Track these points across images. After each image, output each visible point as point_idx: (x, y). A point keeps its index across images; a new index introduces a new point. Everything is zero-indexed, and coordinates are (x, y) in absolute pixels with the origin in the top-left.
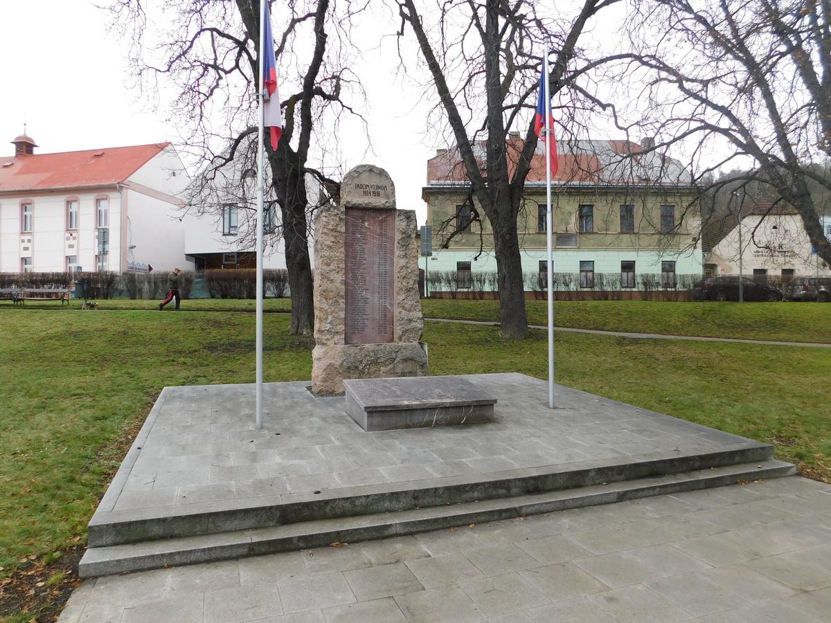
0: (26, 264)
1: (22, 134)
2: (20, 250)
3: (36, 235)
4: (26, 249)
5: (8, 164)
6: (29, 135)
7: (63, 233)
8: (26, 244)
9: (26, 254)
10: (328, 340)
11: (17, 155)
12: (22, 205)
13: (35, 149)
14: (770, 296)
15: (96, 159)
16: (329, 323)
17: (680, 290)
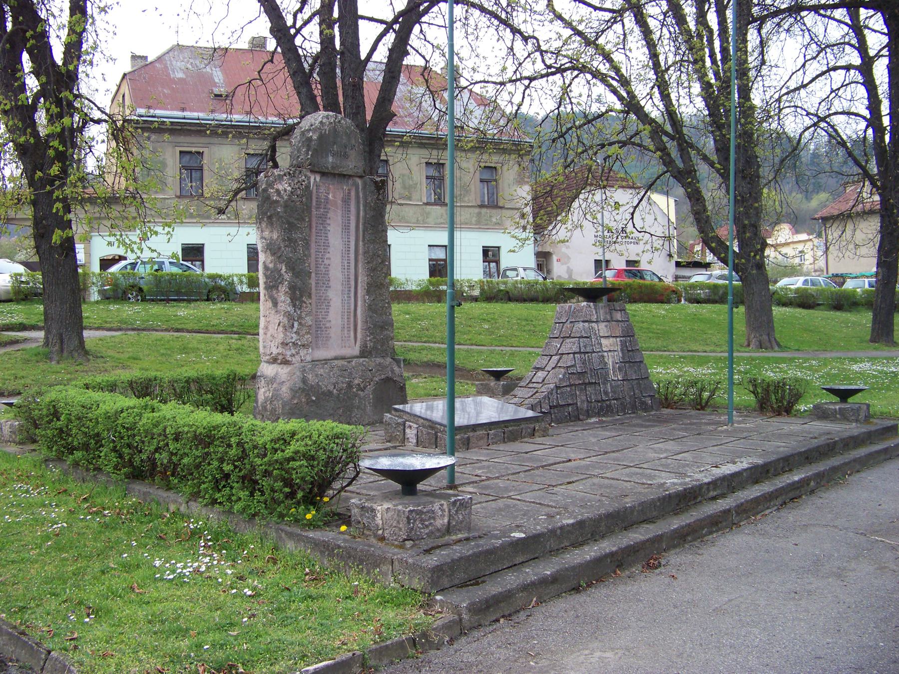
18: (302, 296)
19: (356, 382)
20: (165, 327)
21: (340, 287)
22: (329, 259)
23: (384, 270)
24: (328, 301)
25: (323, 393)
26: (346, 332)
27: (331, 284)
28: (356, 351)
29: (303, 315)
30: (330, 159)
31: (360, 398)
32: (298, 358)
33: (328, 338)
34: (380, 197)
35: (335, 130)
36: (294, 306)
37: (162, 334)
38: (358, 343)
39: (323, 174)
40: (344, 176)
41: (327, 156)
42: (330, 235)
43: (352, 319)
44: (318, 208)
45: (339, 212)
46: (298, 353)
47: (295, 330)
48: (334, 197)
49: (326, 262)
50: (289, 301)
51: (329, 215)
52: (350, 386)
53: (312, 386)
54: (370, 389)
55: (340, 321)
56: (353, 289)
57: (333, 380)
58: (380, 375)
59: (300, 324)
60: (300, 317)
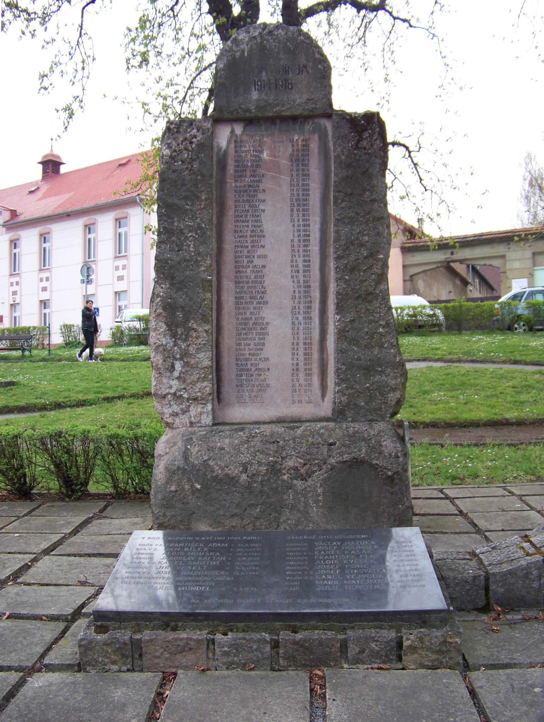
0: (45, 308)
1: (47, 151)
2: (38, 291)
3: (23, 276)
4: (44, 289)
5: (33, 189)
6: (55, 152)
7: (111, 261)
8: (121, 273)
9: (44, 296)
10: (175, 415)
11: (44, 178)
12: (41, 235)
13: (62, 167)
14: (516, 326)
15: (121, 168)
16: (178, 378)
17: (204, 275)
18: (187, 320)
19: (291, 463)
20: (504, 358)
21: (288, 303)
22: (265, 257)
23: (377, 269)
24: (263, 329)
25: (215, 479)
26: (302, 376)
27: (267, 297)
28: (326, 408)
29: (192, 350)
30: (255, 95)
31: (296, 492)
32: (185, 419)
33: (263, 387)
34: (364, 143)
35: (262, 48)
36: (174, 335)
37: (499, 366)
38: (330, 396)
39: (250, 121)
40: (294, 119)
41: (247, 91)
42: (265, 218)
43: (316, 356)
44: (238, 176)
45: (285, 179)
46: (184, 412)
47: (176, 374)
48: (272, 155)
49: (256, 261)
50: (163, 327)
51: (262, 186)
52: (274, 469)
53: (194, 466)
54: (319, 476)
55: (288, 359)
56: (316, 305)
57: (244, 459)
58: (341, 454)
59: (186, 364)
60: (185, 355)
